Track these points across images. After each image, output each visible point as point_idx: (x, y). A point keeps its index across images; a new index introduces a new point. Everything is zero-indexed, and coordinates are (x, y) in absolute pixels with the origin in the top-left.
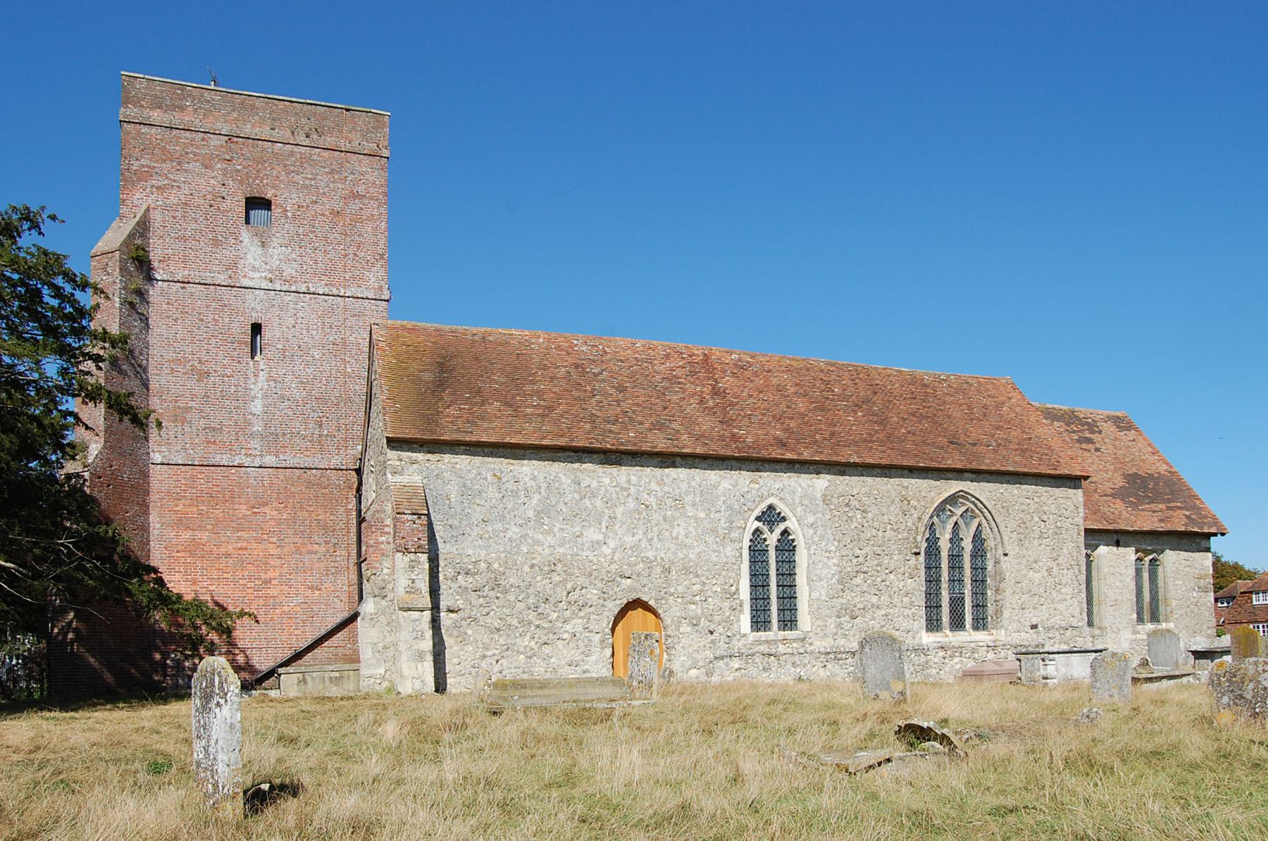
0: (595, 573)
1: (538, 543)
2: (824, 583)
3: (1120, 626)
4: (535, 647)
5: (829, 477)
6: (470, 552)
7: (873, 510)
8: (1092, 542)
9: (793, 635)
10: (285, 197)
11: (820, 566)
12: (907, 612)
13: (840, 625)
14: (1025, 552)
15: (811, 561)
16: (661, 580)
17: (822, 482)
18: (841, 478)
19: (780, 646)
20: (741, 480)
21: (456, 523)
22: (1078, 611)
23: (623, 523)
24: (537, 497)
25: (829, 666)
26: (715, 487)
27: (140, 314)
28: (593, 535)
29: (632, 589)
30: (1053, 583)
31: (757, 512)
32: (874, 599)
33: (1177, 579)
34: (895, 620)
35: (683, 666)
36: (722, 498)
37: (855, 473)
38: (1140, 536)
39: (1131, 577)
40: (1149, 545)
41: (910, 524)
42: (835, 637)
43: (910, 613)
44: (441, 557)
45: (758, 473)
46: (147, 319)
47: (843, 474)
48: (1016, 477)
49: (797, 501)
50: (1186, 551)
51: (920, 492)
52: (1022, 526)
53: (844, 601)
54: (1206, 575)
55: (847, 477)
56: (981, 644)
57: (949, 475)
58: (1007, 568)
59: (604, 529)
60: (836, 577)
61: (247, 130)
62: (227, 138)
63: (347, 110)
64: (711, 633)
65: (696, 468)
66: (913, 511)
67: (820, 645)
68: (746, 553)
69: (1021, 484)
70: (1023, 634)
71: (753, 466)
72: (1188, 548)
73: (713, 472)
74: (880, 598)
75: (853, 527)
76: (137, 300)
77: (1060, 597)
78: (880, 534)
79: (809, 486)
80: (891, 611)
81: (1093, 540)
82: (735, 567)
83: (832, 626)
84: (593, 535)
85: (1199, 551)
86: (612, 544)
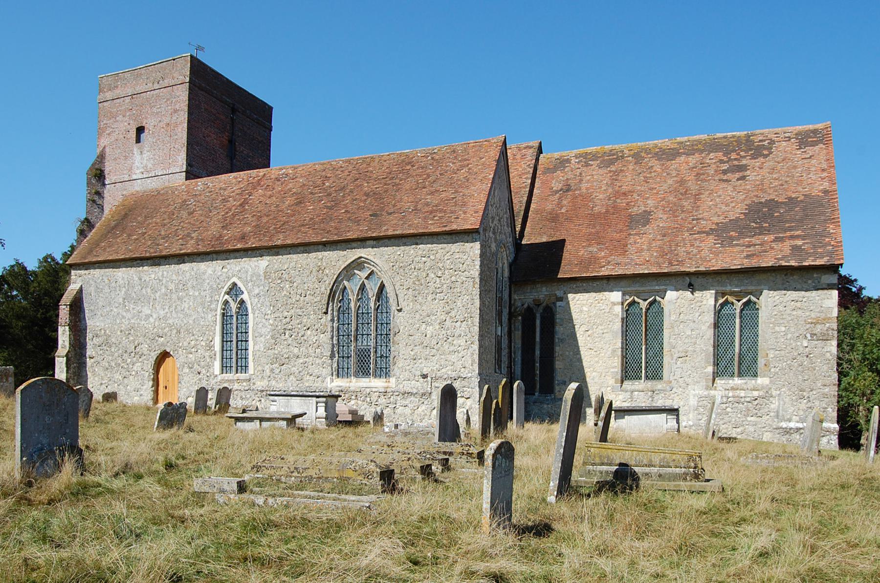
0: (147, 335)
1: (124, 317)
2: (262, 339)
3: (689, 381)
4: (121, 379)
5: (268, 258)
6: (98, 324)
7: (298, 280)
8: (657, 288)
9: (243, 376)
10: (150, 124)
11: (261, 326)
12: (318, 361)
13: (272, 370)
14: (419, 307)
15: (255, 323)
16: (176, 338)
17: (262, 263)
18: (276, 257)
19: (236, 384)
20: (209, 269)
21: (93, 308)
22: (470, 362)
23: (159, 302)
24: (124, 289)
25: (263, 400)
26: (204, 273)
27: (98, 204)
28: (146, 311)
29: (162, 345)
30: (445, 335)
31: (225, 289)
32: (296, 350)
33: (779, 325)
34: (310, 367)
35: (184, 395)
36: (208, 281)
37: (286, 252)
38: (724, 277)
39: (708, 324)
40: (737, 286)
41: (323, 289)
42: (269, 379)
43: (320, 361)
44: (88, 328)
45: (227, 261)
46: (103, 207)
47: (277, 254)
48: (413, 238)
49: (249, 279)
50: (795, 289)
51: (331, 261)
52: (417, 283)
53: (276, 352)
54: (828, 319)
55: (281, 257)
56: (374, 390)
57: (354, 244)
58: (400, 322)
59: (151, 308)
60: (271, 334)
61: (139, 89)
62: (130, 97)
63: (174, 60)
64: (199, 373)
65: (194, 262)
66: (325, 278)
67: (260, 384)
68: (219, 318)
69: (417, 244)
70: (413, 382)
71: (224, 256)
72: (799, 286)
73: (204, 263)
74: (299, 349)
75: (283, 295)
76: (96, 198)
77: (452, 348)
78: (302, 298)
79: (256, 266)
80: (307, 360)
81: (752, 285)
82: (213, 328)
83: (268, 371)
84: (146, 311)
85: (818, 289)
86: (155, 316)
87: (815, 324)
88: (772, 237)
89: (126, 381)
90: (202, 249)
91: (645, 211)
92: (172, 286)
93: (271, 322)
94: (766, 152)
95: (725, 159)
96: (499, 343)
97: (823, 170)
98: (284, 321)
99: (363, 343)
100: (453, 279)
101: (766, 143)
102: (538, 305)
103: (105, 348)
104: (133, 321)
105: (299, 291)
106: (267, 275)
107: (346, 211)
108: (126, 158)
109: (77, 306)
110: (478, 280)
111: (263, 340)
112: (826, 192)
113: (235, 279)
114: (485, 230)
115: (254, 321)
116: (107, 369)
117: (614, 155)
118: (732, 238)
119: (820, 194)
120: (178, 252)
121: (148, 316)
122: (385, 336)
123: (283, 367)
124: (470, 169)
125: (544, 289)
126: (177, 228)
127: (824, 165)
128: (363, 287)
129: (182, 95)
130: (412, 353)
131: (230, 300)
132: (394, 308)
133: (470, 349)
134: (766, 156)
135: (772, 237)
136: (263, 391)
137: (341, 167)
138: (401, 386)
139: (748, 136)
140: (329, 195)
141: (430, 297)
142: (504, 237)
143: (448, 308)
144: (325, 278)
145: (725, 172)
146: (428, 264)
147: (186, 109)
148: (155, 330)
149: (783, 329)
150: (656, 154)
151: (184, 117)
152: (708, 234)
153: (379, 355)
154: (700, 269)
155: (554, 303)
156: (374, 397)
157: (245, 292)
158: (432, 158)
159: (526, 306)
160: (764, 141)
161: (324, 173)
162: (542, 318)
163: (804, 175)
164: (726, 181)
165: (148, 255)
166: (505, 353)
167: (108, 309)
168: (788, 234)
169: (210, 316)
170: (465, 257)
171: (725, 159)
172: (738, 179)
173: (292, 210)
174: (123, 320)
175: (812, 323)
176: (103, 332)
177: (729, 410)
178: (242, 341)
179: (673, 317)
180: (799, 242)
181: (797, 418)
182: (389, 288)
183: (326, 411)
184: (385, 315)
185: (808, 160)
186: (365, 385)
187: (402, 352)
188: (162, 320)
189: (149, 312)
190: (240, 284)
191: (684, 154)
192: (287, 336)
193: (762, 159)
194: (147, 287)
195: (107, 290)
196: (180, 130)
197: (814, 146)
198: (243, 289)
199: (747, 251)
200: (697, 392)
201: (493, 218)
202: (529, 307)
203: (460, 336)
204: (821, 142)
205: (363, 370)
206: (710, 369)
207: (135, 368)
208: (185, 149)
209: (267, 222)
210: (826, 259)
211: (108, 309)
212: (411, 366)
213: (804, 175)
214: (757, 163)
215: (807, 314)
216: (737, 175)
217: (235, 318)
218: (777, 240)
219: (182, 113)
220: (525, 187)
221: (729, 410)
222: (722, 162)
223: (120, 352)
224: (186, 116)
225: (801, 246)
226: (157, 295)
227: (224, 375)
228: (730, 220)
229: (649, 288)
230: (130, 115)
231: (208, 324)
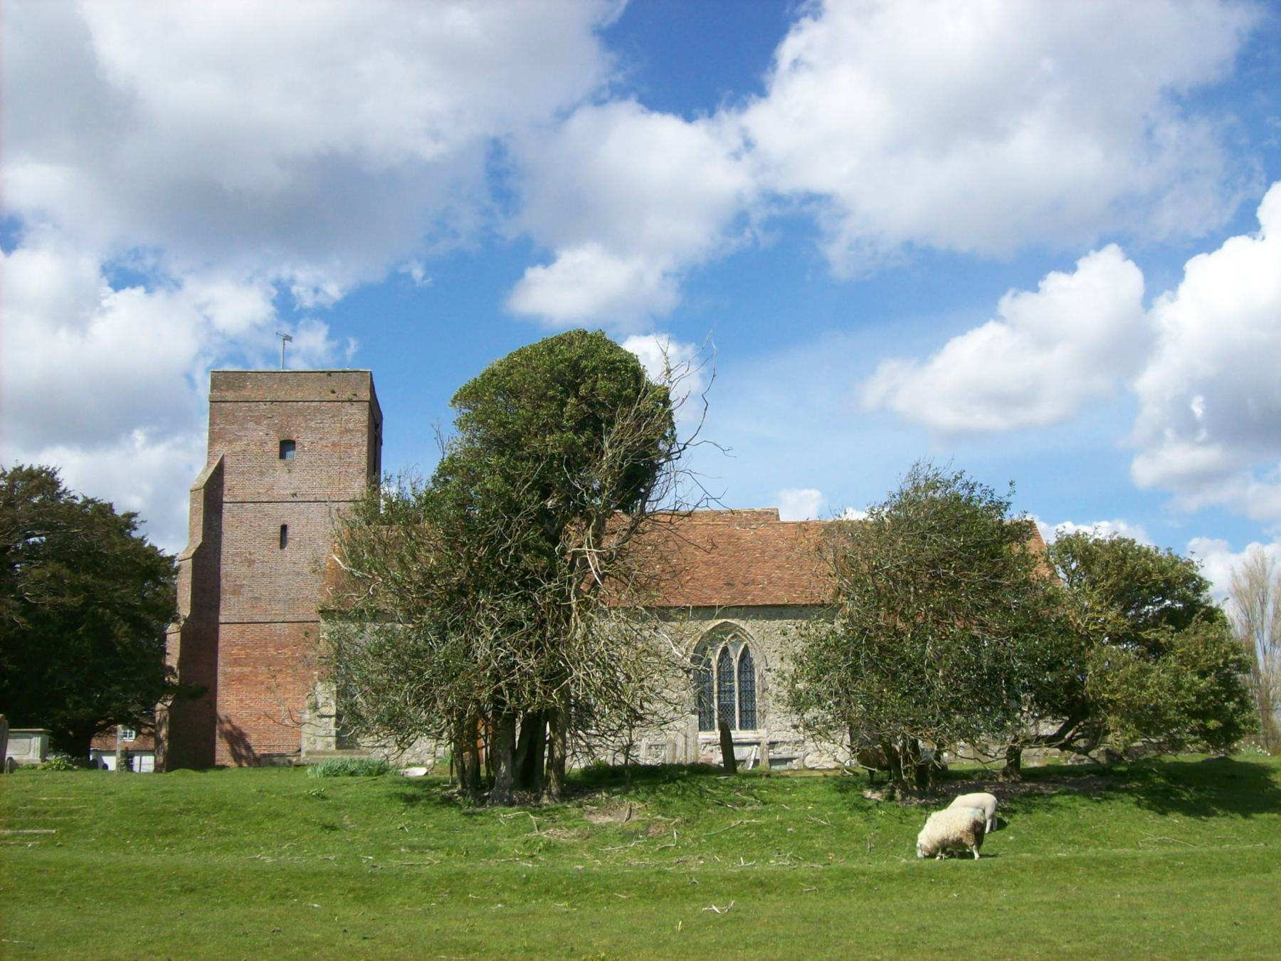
10: (304, 439)
108: (262, 474)
128: (725, 651)
138: (773, 736)
158: (755, 534)
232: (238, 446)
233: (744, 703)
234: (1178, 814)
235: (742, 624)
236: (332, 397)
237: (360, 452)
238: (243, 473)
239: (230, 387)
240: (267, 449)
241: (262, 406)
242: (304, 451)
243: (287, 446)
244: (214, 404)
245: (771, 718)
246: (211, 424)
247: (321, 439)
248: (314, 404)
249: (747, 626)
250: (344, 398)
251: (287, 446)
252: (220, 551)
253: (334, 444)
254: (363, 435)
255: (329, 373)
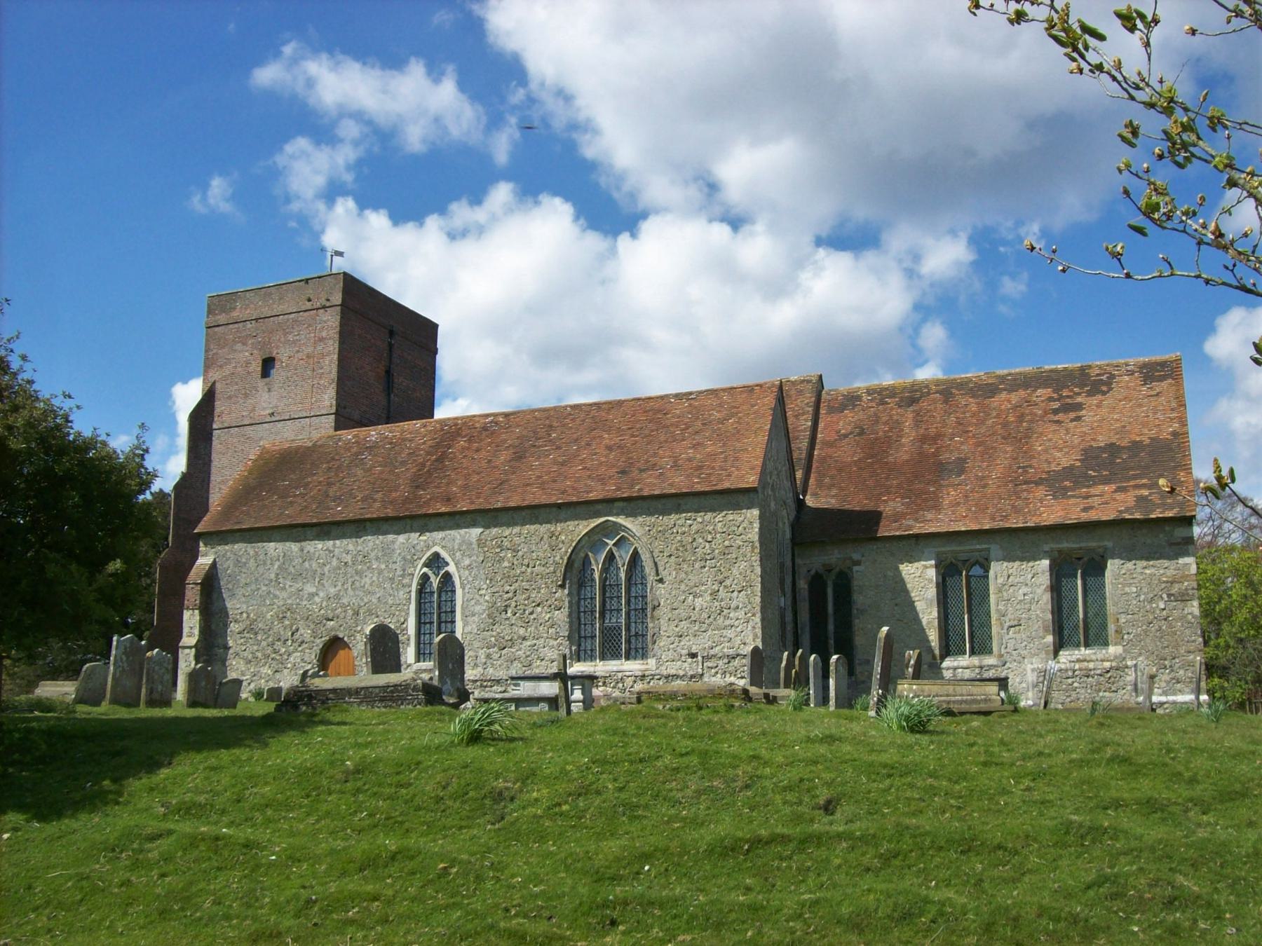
1: (276, 597)
2: (476, 619)
3: (1024, 652)
7: (524, 549)
8: (978, 547)
10: (283, 354)
12: (552, 642)
13: (488, 656)
28: (310, 589)
32: (522, 631)
41: (557, 559)
56: (627, 674)
66: (561, 545)
70: (679, 663)
78: (529, 570)
84: (310, 589)
86: (321, 594)
87: (1172, 583)
88: (1114, 487)
89: (278, 676)
90: (390, 512)
91: (958, 459)
92: (348, 558)
93: (487, 598)
94: (1104, 388)
95: (1055, 396)
96: (782, 616)
97: (1172, 410)
98: (506, 596)
99: (611, 621)
100: (727, 543)
101: (1104, 378)
102: (830, 571)
103: (247, 635)
104: (289, 601)
105: (526, 562)
106: (481, 543)
107: (584, 468)
108: (246, 396)
109: (211, 582)
110: (757, 544)
111: (477, 620)
112: (1175, 434)
113: (437, 549)
114: (764, 488)
115: (463, 597)
116: (250, 661)
117: (916, 391)
118: (1066, 489)
119: (1169, 437)
120: (359, 517)
121: (312, 595)
122: (640, 609)
123: (504, 652)
124: (740, 418)
125: (836, 551)
126: (350, 488)
127: (1174, 404)
128: (611, 557)
129: (331, 321)
130: (677, 629)
131: (430, 573)
132: (651, 578)
133: (751, 623)
134: (1104, 393)
135: (1114, 487)
136: (476, 681)
137: (570, 414)
138: (664, 668)
139: (1082, 369)
140: (559, 448)
141: (697, 565)
142: (783, 492)
143: (721, 577)
144: (561, 545)
145: (1056, 412)
146: (694, 528)
147: (337, 336)
148: (322, 612)
149: (1134, 590)
150: (971, 389)
151: (332, 347)
152: (1037, 483)
153: (633, 633)
154: (1028, 524)
155: (850, 569)
156: (629, 681)
157: (452, 564)
158: (690, 405)
159: (813, 572)
160: (1103, 375)
161: (547, 422)
162: (836, 585)
163: (1151, 415)
164: (1058, 422)
165: (315, 521)
166: (789, 627)
167: (253, 587)
168: (1132, 483)
169: (402, 593)
170: (742, 519)
171: (1055, 396)
172: (1072, 421)
173: (510, 467)
174: (275, 601)
175: (1167, 582)
176: (245, 615)
177: (1076, 685)
178: (446, 622)
179: (1000, 581)
180: (1145, 492)
181: (1160, 691)
182: (645, 557)
183: (583, 694)
184: (640, 586)
185: (1155, 398)
186: (615, 669)
187: (663, 628)
188: (332, 600)
189: (314, 590)
190: (444, 554)
191: (1005, 390)
192: (509, 614)
193: (1100, 397)
194: (310, 559)
195: (252, 563)
196: (327, 362)
197: (1162, 381)
198: (448, 559)
199: (1083, 503)
200: (1036, 666)
201: (771, 473)
202: (817, 573)
203: (737, 607)
204: (1170, 376)
205: (610, 651)
206: (1050, 639)
207: (292, 659)
208: (334, 385)
209: (479, 481)
210: (1176, 510)
211: (253, 587)
212: (676, 644)
213: (1151, 415)
214: (1094, 400)
215: (1161, 572)
216: (1072, 415)
217: (436, 595)
218: (1119, 490)
219: (331, 342)
220: (805, 430)
221: (1076, 685)
222: (1051, 399)
223: (270, 639)
224: (337, 345)
225: (1147, 496)
226: (326, 569)
227: (421, 664)
228: (1064, 468)
229: (968, 548)
230: (253, 344)
231: (398, 602)
232: (228, 370)
233: (633, 625)
234: (292, 733)
235: (620, 520)
236: (309, 305)
237: (331, 361)
238: (230, 397)
239: (224, 310)
240: (251, 369)
241: (249, 325)
242: (282, 367)
243: (268, 365)
244: (770, 400)
245: (662, 644)
246: (206, 351)
247: (298, 351)
248: (293, 316)
249: (635, 526)
250: (318, 305)
251: (268, 365)
252: (209, 480)
253: (308, 356)
254: (335, 342)
255: (307, 281)
